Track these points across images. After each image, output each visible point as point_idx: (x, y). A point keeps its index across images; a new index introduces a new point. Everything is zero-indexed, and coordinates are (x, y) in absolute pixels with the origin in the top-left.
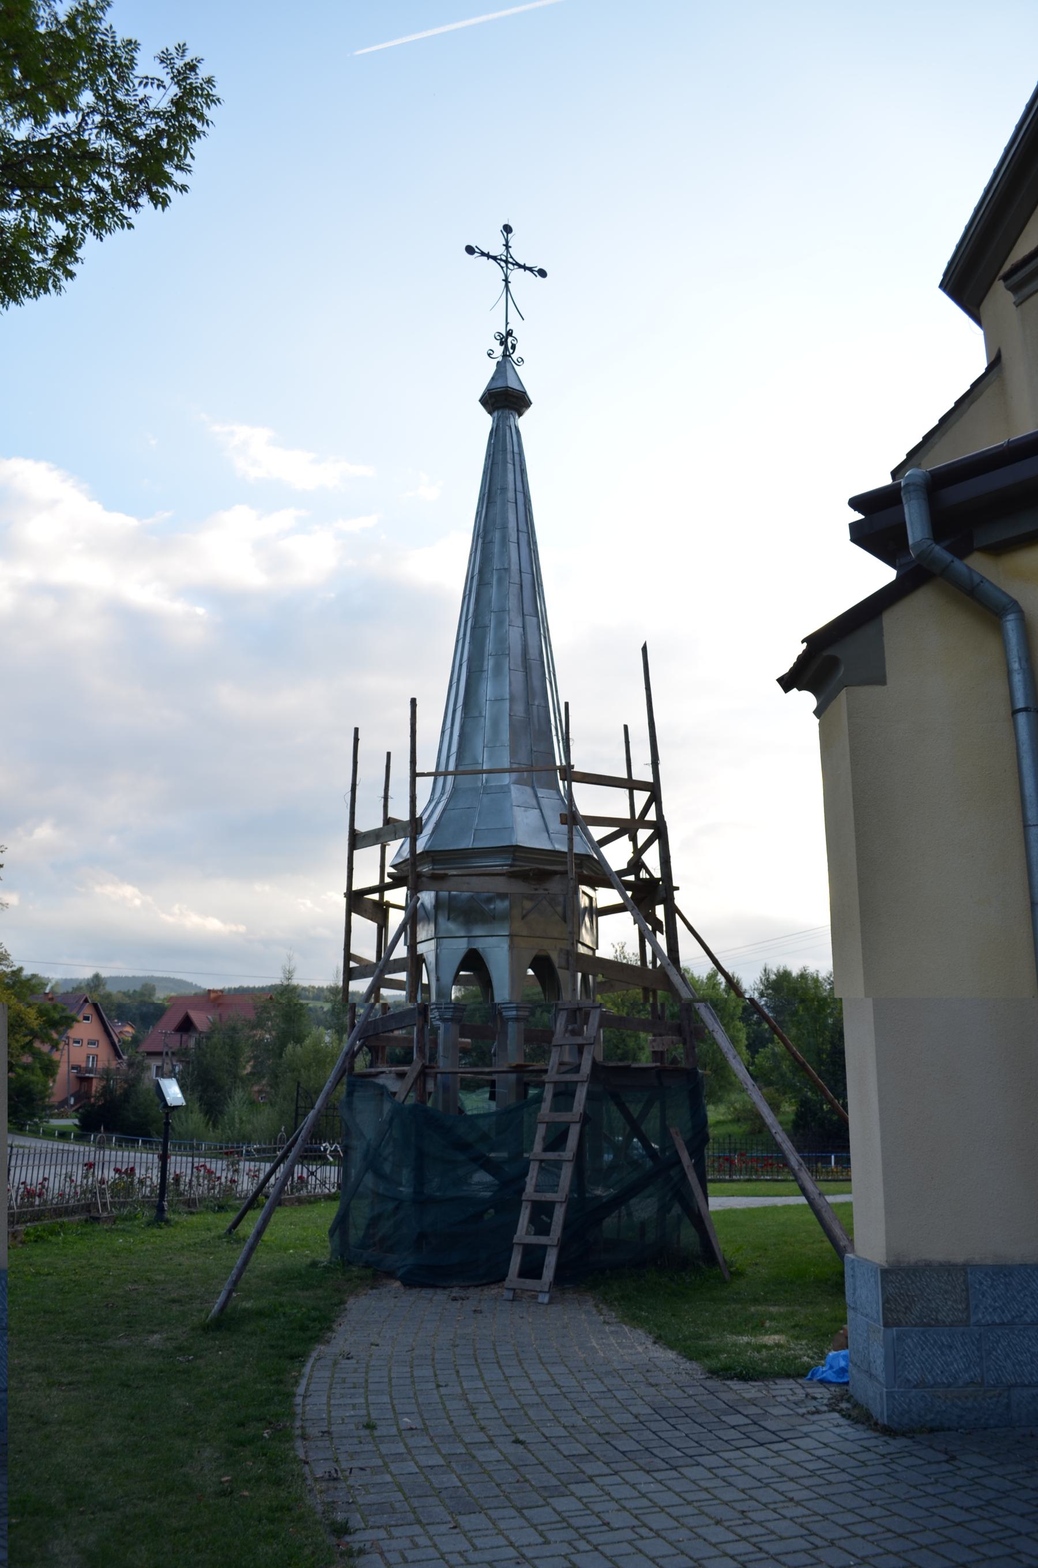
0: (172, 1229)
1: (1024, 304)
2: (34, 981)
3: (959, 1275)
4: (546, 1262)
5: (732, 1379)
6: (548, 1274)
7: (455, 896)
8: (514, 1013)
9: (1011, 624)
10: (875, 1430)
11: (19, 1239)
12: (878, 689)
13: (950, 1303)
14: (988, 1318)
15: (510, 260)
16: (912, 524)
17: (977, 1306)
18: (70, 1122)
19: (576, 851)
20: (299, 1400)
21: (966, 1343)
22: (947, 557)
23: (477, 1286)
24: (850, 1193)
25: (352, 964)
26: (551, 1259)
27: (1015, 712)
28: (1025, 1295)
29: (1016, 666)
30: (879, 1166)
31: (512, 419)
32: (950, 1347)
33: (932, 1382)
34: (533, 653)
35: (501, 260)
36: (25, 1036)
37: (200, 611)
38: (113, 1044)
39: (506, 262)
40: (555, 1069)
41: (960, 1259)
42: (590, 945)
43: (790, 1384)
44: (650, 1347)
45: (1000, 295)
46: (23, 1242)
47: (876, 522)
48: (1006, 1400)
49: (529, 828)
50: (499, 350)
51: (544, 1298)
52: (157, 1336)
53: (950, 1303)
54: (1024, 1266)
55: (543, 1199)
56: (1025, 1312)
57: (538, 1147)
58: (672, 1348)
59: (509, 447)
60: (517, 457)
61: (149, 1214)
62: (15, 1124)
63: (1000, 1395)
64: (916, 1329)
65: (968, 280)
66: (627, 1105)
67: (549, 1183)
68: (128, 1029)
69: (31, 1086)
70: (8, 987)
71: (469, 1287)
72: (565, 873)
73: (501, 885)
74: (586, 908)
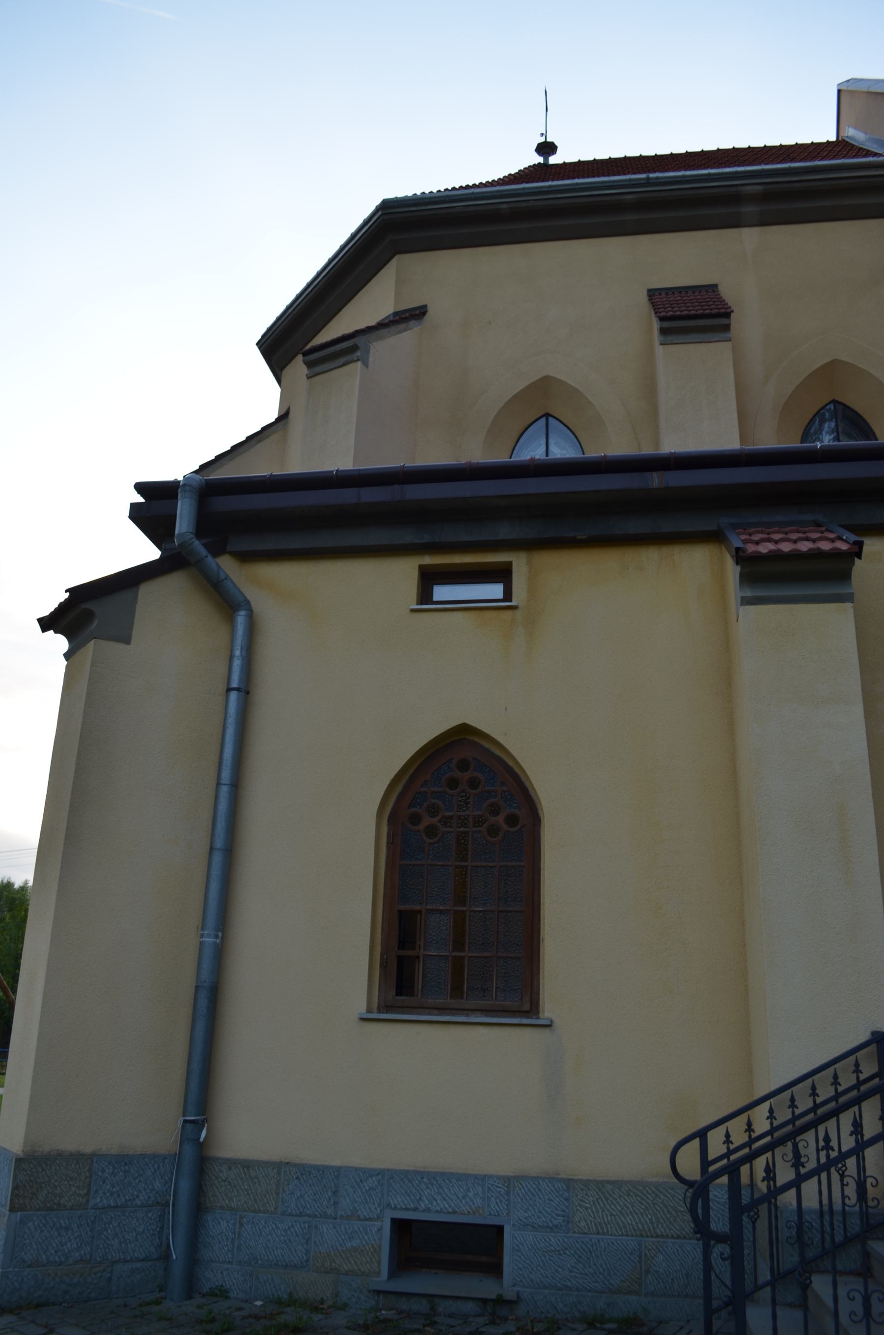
1: (313, 379)
9: (241, 618)
12: (121, 646)
13: (73, 1189)
14: (105, 1202)
16: (181, 517)
17: (96, 1192)
22: (203, 551)
27: (229, 690)
29: (237, 653)
30: (32, 1064)
41: (88, 1150)
45: (298, 367)
47: (154, 507)
48: (109, 1275)
53: (73, 1189)
54: (143, 1156)
56: (138, 1196)
63: (104, 1270)
64: (39, 1213)
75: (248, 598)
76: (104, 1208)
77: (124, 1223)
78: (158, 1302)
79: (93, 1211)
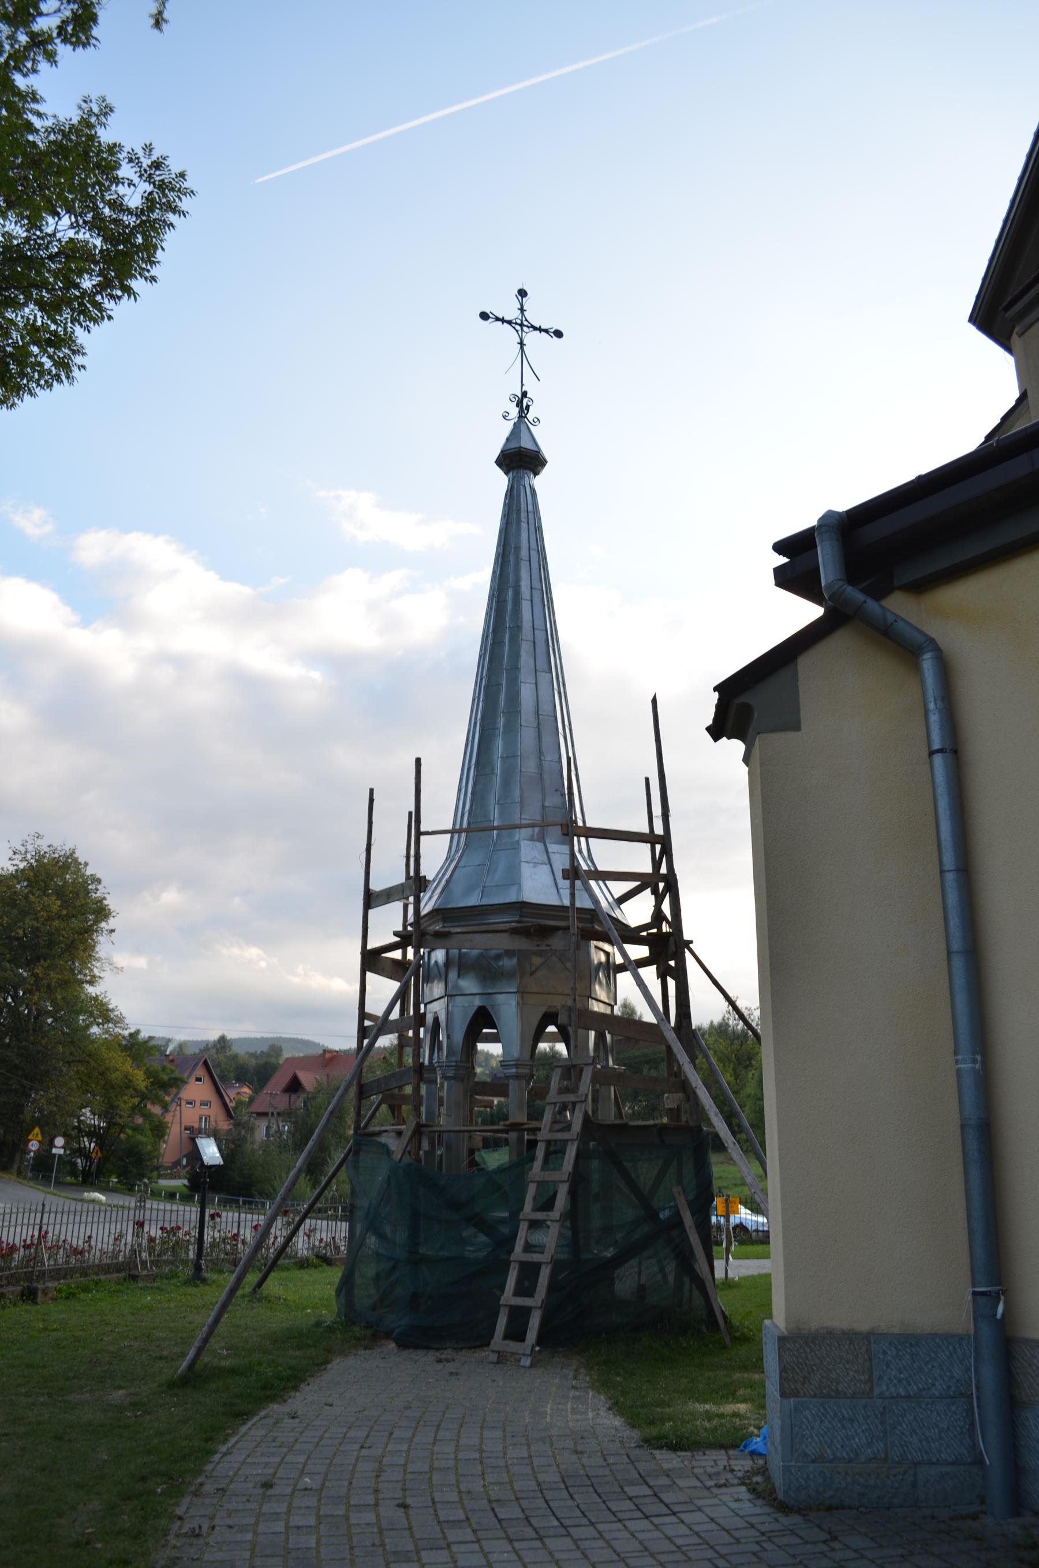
0: (207, 1288)
1: (1027, 334)
2: (152, 1043)
3: (861, 1343)
4: (530, 1325)
5: (661, 1448)
6: (532, 1336)
7: (465, 954)
8: (514, 1070)
9: (927, 663)
10: (772, 1506)
11: (50, 1295)
12: (791, 735)
14: (892, 1390)
15: (525, 323)
17: (880, 1377)
18: (179, 1183)
19: (578, 905)
20: (217, 1457)
21: (868, 1417)
23: (470, 1348)
24: (767, 1256)
25: (367, 1023)
26: (535, 1322)
27: (931, 753)
28: (933, 1367)
29: (932, 706)
31: (526, 478)
32: (851, 1420)
33: (831, 1457)
34: (545, 709)
35: (516, 323)
36: (132, 1097)
37: (316, 675)
38: (225, 1105)
39: (521, 325)
40: (548, 1127)
41: (864, 1327)
42: (606, 1001)
43: (720, 1457)
44: (601, 1413)
46: (54, 1299)
47: (798, 563)
49: (538, 885)
50: (514, 412)
51: (526, 1362)
52: (121, 1392)
54: (934, 1336)
55: (530, 1260)
56: (933, 1385)
57: (528, 1207)
58: (622, 1415)
59: (523, 506)
60: (531, 515)
61: (190, 1271)
62: (125, 1184)
63: (905, 1472)
64: (816, 1400)
65: (999, 311)
66: (625, 1163)
67: (542, 1241)
68: (246, 1090)
69: (141, 1147)
70: (125, 1049)
71: (462, 1349)
72: (567, 928)
73: (504, 942)
74: (600, 963)
75: (933, 636)
76: (893, 1398)
77: (921, 1416)
78: (975, 1517)
79: (880, 1401)
